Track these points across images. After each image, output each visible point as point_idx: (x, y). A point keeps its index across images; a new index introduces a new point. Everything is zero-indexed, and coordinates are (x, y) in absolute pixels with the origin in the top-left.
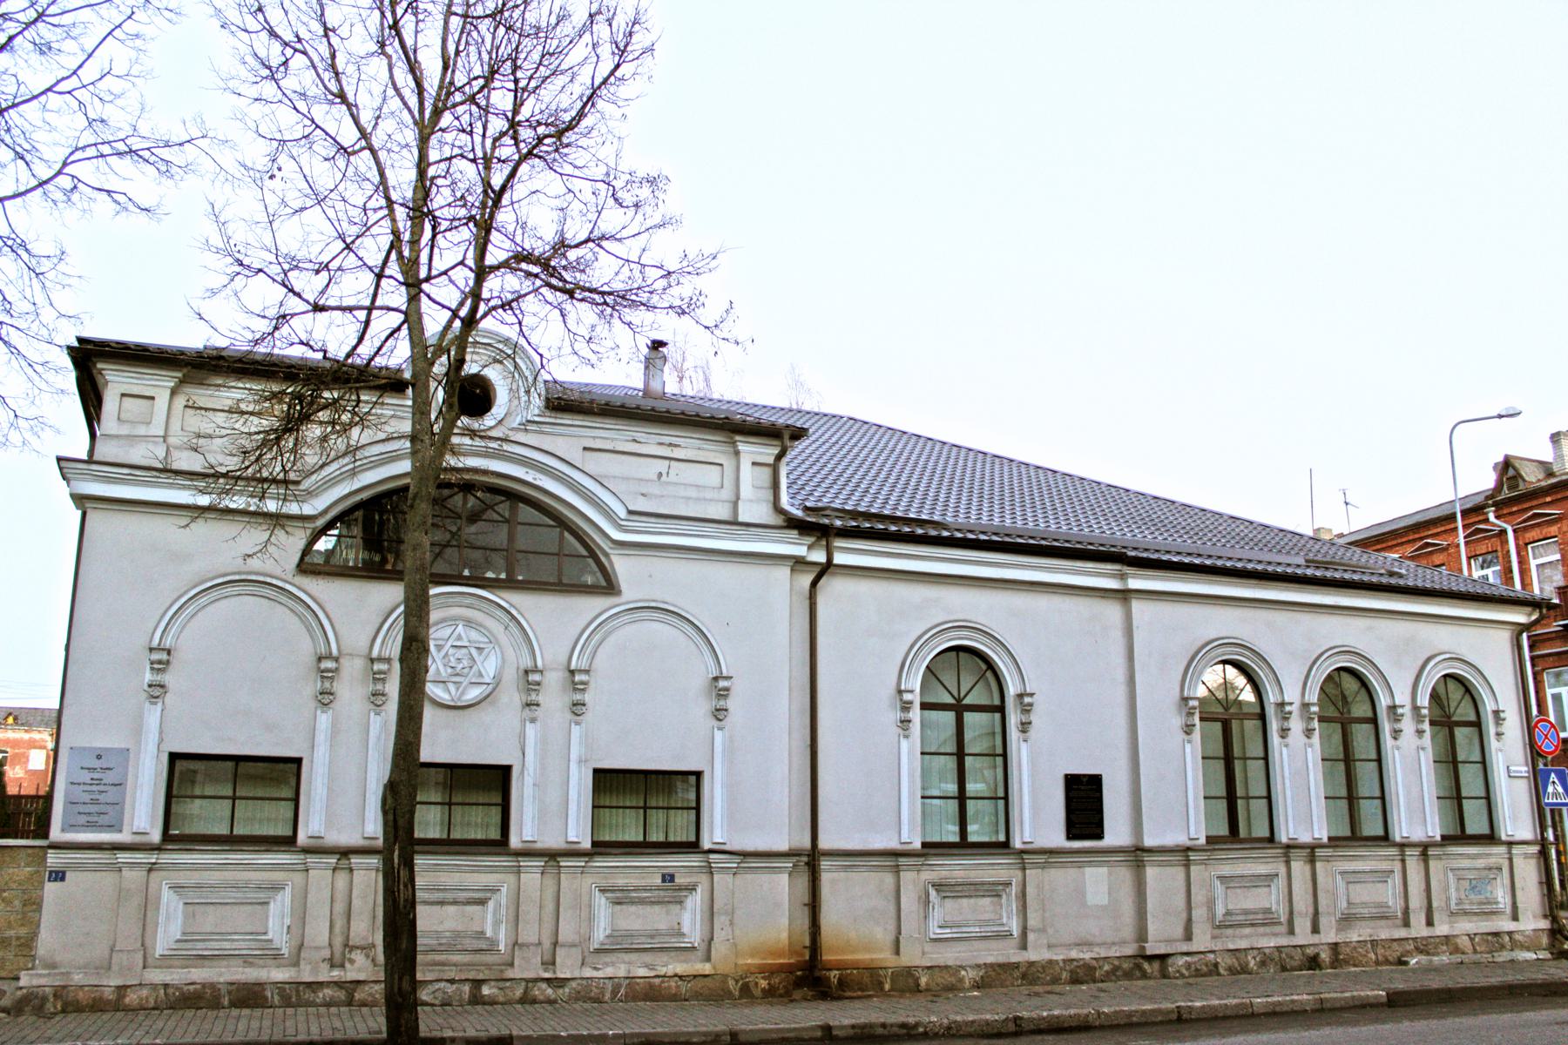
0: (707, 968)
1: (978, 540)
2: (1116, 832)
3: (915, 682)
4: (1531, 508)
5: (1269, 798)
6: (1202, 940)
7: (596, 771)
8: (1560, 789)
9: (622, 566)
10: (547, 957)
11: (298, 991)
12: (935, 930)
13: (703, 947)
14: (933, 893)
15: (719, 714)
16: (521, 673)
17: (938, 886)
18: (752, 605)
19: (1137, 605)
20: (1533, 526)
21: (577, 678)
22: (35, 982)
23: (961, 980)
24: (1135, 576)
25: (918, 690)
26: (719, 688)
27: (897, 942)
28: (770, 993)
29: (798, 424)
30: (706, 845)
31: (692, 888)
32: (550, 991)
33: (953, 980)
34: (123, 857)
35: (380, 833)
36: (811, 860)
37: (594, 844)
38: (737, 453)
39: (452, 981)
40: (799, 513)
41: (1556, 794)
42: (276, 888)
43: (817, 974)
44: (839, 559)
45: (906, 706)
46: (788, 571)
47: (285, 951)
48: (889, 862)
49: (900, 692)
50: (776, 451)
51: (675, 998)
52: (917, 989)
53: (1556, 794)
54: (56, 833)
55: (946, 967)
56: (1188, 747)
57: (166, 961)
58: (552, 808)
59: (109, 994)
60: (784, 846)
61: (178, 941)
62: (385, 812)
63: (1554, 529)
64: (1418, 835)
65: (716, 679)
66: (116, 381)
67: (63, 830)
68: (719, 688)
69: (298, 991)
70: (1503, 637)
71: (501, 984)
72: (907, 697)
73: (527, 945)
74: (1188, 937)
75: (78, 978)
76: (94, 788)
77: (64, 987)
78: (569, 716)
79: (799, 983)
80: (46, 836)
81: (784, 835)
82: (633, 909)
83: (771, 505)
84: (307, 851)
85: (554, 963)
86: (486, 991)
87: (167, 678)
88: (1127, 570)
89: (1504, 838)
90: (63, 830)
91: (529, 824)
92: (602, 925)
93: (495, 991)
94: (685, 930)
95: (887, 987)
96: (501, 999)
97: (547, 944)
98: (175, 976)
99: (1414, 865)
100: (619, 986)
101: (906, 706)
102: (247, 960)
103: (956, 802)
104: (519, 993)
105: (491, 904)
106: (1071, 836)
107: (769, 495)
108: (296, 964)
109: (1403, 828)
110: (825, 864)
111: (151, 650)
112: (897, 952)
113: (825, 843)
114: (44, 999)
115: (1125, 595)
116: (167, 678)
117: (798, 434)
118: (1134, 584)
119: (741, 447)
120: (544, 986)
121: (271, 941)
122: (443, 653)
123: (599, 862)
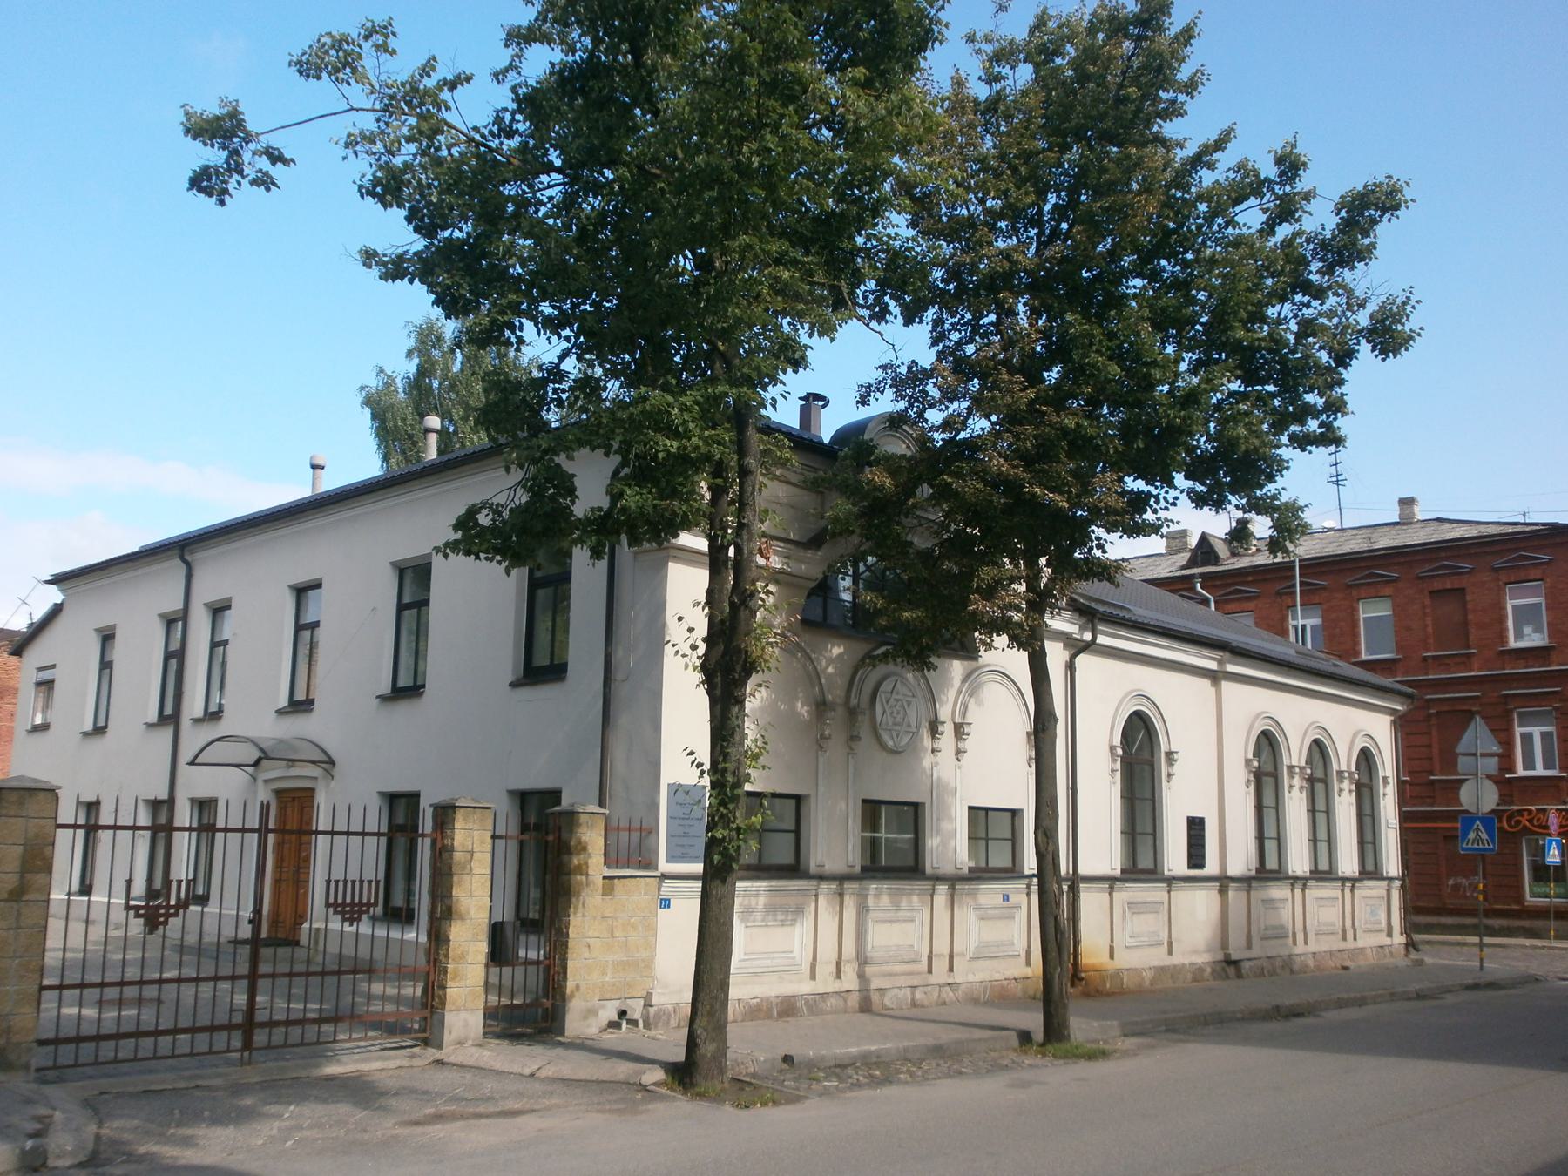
2: (1211, 867)
5: (1278, 839)
6: (1256, 951)
7: (970, 808)
8: (1484, 836)
13: (1023, 954)
19: (1226, 685)
27: (1112, 949)
31: (1018, 907)
41: (1478, 840)
53: (1478, 840)
54: (664, 866)
64: (1299, 873)
74: (1249, 946)
87: (615, 1018)
88: (1227, 655)
106: (1190, 867)
109: (1027, 872)
112: (1112, 957)
113: (1082, 870)
115: (1215, 677)
116: (615, 1018)
118: (1230, 668)
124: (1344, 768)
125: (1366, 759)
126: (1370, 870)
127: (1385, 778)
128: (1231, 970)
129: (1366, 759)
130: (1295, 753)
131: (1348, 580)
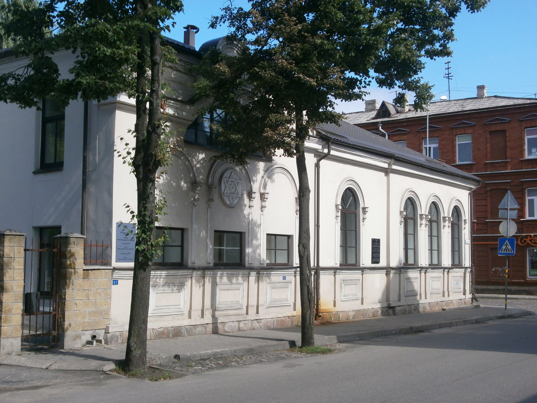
2: (383, 263)
4: (398, 127)
6: (402, 303)
20: (396, 135)
24: (394, 164)
27: (335, 302)
39: (233, 322)
41: (506, 249)
44: (333, 152)
53: (506, 249)
63: (405, 137)
67: (116, 262)
70: (467, 192)
74: (399, 300)
76: (125, 242)
89: (190, 265)
90: (116, 262)
94: (289, 299)
99: (423, 274)
103: (180, 248)
112: (335, 306)
113: (321, 265)
118: (394, 167)
124: (446, 215)
125: (457, 211)
126: (457, 264)
127: (465, 220)
128: (391, 311)
129: (457, 211)
130: (424, 209)
131: (452, 126)
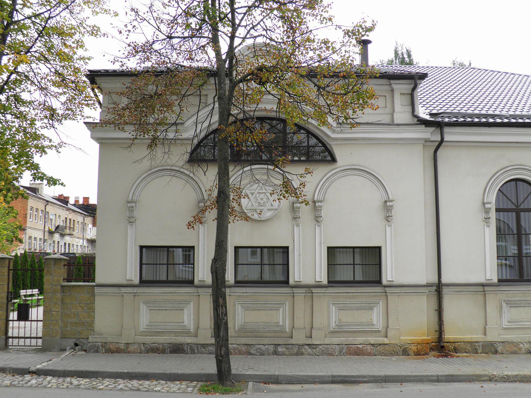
0: (386, 341)
1: (524, 123)
3: (492, 198)
7: (328, 248)
9: (338, 152)
10: (308, 335)
11: (197, 348)
12: (505, 323)
14: (504, 305)
15: (388, 219)
16: (291, 203)
17: (508, 303)
18: (404, 171)
21: (317, 204)
22: (95, 340)
23: (520, 349)
25: (494, 202)
26: (387, 208)
28: (418, 354)
29: (425, 72)
30: (384, 282)
32: (309, 350)
33: (516, 349)
34: (123, 290)
35: (211, 282)
36: (438, 289)
37: (329, 282)
38: (392, 90)
40: (428, 117)
42: (187, 303)
43: (442, 344)
45: (487, 211)
46: (421, 147)
47: (192, 330)
48: (480, 289)
49: (484, 204)
50: (412, 86)
51: (369, 354)
52: (496, 352)
55: (512, 342)
56: (487, 230)
57: (144, 334)
58: (308, 266)
59: (122, 347)
60: (424, 282)
61: (147, 325)
62: (212, 273)
65: (386, 202)
66: (98, 80)
68: (387, 208)
69: (197, 348)
71: (287, 346)
72: (488, 206)
73: (299, 329)
75: (110, 340)
77: (105, 343)
78: (315, 222)
79: (432, 349)
80: (93, 281)
81: (424, 275)
82: (348, 312)
83: (410, 114)
84: (197, 287)
85: (311, 337)
86: (280, 349)
91: (298, 273)
92: (334, 321)
93: (285, 349)
95: (480, 351)
96: (287, 353)
97: (308, 327)
98: (148, 340)
100: (343, 348)
101: (487, 211)
102: (177, 334)
104: (295, 350)
105: (281, 310)
107: (409, 108)
108: (197, 336)
110: (445, 290)
111: (129, 202)
113: (444, 280)
114: (98, 347)
117: (423, 76)
119: (394, 86)
120: (307, 347)
121: (185, 326)
122: (254, 196)
123: (331, 290)
